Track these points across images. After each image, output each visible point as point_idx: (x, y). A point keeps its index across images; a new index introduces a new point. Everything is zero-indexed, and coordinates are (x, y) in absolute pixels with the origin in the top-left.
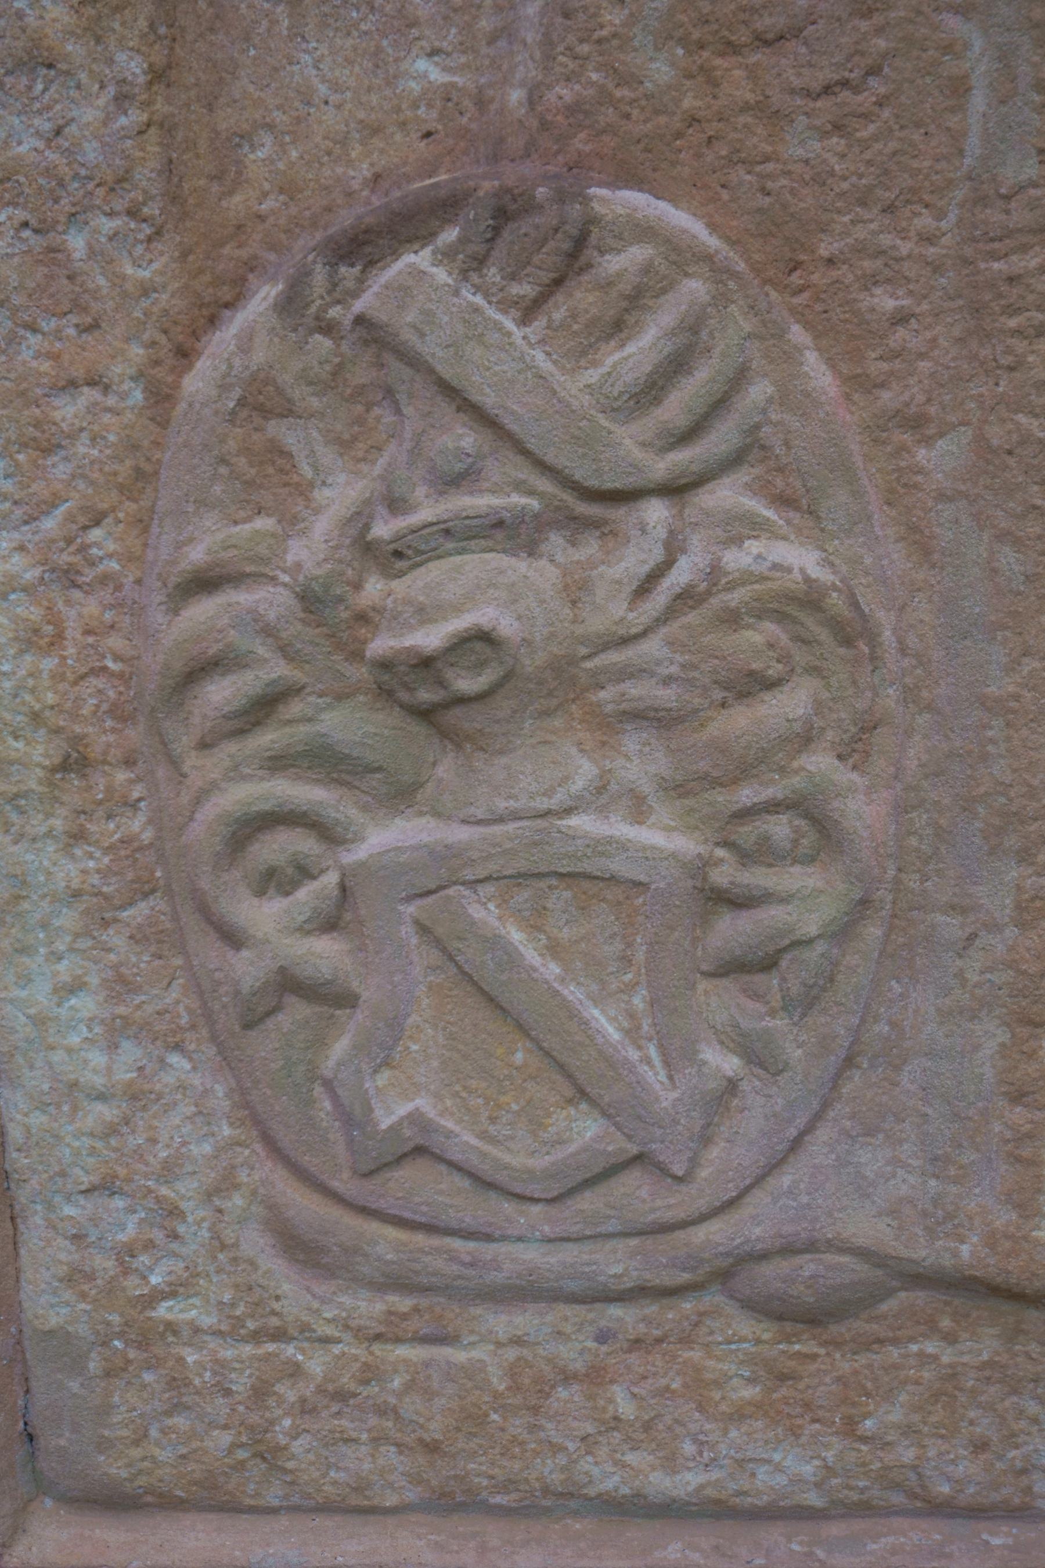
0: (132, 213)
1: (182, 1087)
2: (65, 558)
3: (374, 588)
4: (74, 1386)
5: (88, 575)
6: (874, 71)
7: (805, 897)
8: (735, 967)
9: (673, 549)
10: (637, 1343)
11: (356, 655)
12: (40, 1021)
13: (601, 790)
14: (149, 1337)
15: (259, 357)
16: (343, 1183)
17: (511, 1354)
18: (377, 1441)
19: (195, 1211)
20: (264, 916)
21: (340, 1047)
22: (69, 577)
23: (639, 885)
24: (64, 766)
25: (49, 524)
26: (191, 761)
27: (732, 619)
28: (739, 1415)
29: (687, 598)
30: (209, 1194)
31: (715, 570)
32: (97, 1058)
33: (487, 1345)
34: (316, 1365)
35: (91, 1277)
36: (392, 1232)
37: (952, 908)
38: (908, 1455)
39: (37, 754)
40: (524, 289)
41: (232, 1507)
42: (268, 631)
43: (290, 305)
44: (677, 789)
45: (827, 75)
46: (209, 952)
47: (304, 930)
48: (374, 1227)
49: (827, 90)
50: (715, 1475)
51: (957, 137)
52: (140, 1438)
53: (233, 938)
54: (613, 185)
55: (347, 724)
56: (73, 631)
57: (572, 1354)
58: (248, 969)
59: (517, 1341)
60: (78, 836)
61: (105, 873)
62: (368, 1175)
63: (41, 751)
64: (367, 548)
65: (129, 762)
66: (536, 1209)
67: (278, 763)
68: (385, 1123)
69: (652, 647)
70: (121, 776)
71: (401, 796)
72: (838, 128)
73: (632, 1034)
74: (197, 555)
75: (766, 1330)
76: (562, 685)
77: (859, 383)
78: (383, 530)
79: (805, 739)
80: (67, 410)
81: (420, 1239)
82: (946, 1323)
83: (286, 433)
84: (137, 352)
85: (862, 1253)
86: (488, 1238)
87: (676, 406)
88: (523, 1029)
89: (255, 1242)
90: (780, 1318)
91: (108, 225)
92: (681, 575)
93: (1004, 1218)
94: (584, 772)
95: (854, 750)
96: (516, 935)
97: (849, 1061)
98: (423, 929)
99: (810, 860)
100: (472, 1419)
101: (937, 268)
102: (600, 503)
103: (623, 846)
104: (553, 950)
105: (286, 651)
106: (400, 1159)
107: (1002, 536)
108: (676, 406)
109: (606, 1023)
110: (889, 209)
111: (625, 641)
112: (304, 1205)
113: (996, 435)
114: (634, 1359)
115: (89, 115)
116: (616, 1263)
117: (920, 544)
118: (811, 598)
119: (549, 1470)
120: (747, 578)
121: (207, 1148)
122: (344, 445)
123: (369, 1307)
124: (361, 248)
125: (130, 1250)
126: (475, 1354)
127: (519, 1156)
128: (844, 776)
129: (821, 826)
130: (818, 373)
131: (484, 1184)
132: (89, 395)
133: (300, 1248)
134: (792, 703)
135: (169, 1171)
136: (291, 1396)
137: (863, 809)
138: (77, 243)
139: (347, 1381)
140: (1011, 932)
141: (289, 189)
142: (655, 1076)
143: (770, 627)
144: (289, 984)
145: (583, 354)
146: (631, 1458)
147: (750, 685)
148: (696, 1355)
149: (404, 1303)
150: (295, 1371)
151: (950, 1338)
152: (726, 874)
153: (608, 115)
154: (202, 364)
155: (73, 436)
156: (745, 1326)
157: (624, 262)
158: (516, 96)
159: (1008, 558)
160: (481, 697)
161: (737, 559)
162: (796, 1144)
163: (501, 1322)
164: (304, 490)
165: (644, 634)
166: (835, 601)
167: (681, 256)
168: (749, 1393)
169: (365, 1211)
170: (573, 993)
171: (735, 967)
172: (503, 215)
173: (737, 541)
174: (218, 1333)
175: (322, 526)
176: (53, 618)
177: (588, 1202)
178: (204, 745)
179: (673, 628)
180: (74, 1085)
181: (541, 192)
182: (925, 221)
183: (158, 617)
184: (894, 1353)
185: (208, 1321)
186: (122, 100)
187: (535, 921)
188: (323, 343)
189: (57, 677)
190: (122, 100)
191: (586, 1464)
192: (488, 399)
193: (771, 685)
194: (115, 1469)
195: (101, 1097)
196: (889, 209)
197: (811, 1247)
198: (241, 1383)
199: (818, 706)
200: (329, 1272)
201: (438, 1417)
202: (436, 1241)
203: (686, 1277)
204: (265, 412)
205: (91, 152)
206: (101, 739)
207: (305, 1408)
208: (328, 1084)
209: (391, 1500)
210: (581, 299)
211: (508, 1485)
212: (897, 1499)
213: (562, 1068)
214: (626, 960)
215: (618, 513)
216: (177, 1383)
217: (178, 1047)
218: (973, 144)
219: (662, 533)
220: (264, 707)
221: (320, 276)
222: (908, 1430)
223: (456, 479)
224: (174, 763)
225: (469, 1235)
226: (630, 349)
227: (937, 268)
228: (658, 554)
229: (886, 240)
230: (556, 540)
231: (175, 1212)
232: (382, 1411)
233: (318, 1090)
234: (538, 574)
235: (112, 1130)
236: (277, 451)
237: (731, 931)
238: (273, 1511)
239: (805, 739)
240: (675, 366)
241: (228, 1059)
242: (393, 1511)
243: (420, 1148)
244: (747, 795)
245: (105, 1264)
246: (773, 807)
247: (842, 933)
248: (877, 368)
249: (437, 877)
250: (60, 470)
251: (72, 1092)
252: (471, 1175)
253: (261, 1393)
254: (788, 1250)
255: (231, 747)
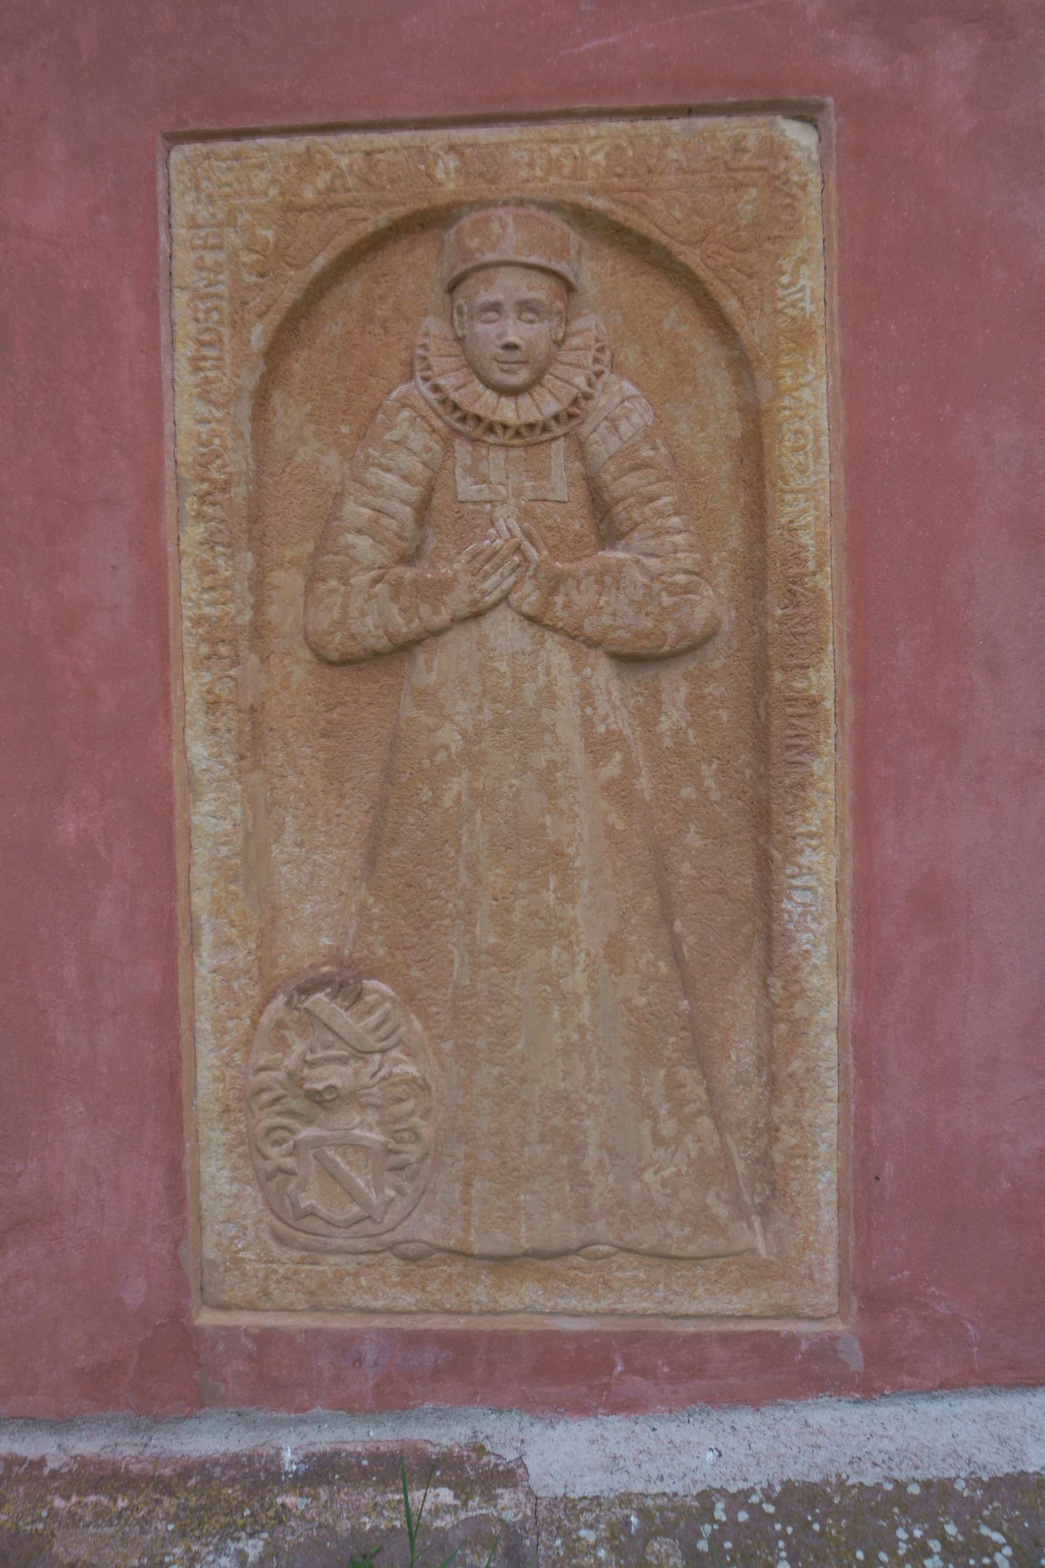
0: (250, 979)
1: (250, 1195)
2: (227, 1060)
3: (306, 1071)
4: (215, 1275)
5: (233, 1065)
6: (432, 957)
7: (412, 1152)
8: (393, 1169)
9: (381, 1066)
10: (368, 1266)
11: (301, 1087)
12: (213, 1177)
13: (361, 1123)
14: (237, 1262)
15: (280, 1015)
16: (291, 1221)
17: (334, 1268)
18: (297, 1291)
19: (251, 1228)
20: (274, 1152)
21: (292, 1186)
22: (228, 1065)
23: (370, 1148)
24: (224, 1111)
25: (224, 1051)
26: (256, 1113)
27: (394, 1085)
28: (395, 1285)
29: (383, 1079)
30: (255, 1224)
31: (390, 1073)
32: (227, 1187)
33: (328, 1265)
34: (281, 1270)
35: (222, 1245)
36: (303, 1235)
37: (449, 1155)
38: (439, 1297)
39: (217, 1108)
40: (346, 1004)
41: (256, 1309)
42: (279, 1082)
43: (289, 1003)
44: (380, 1124)
45: (420, 957)
46: (259, 1161)
47: (285, 1156)
48: (298, 1233)
49: (421, 961)
50: (388, 1301)
51: (452, 972)
52: (232, 1290)
53: (265, 1157)
54: (369, 979)
55: (297, 1104)
56: (228, 1077)
57: (351, 1268)
58: (269, 1166)
59: (336, 1265)
60: (226, 1129)
61: (233, 1139)
62: (298, 1219)
63: (218, 1107)
64: (305, 1062)
65: (241, 1111)
66: (342, 1230)
67: (279, 1114)
68: (303, 1206)
69: (375, 1090)
70: (238, 1115)
71: (310, 1121)
72: (423, 969)
73: (368, 1185)
74: (262, 1062)
75: (402, 1263)
76: (352, 1098)
77: (427, 1028)
78: (309, 1057)
79: (412, 1113)
80: (230, 1024)
81: (311, 1237)
82: (448, 1261)
83: (286, 1033)
84: (249, 1012)
85: (426, 1243)
86: (329, 1237)
87: (383, 1032)
88: (340, 1183)
89: (267, 1237)
90: (405, 1259)
91: (243, 981)
92: (383, 1072)
93: (461, 1234)
94: (357, 1119)
95: (425, 1116)
96: (339, 1159)
97: (423, 1193)
98: (315, 1156)
99: (414, 1142)
100: (323, 1285)
101: (447, 1001)
102: (362, 1054)
103: (367, 1138)
104: (348, 1163)
105: (283, 1087)
106: (306, 1216)
107: (461, 1066)
108: (383, 1032)
109: (361, 1183)
110: (435, 988)
111: (368, 1087)
112: (280, 1227)
113: (460, 1042)
114: (367, 1270)
115: (241, 956)
116: (362, 1244)
117: (442, 1066)
118: (414, 1080)
119: (343, 1300)
120: (398, 1075)
121: (255, 1211)
122: (300, 1036)
123: (296, 1255)
124: (307, 990)
125: (233, 1238)
126: (325, 1268)
127: (337, 1215)
128: (422, 1122)
129: (417, 1137)
130: (417, 1025)
131: (328, 1223)
132: (236, 1021)
133: (278, 1238)
134: (409, 1105)
135: (244, 1217)
136: (274, 1278)
137: (427, 1131)
138: (235, 985)
139: (289, 1274)
140: (463, 1162)
141: (289, 968)
142: (373, 1196)
143: (405, 1087)
144: (280, 1170)
145: (360, 1019)
146: (366, 1297)
147: (399, 1100)
148: (383, 1269)
149: (306, 1254)
150: (276, 1272)
151: (450, 1266)
152: (392, 1145)
153: (368, 962)
154: (265, 1015)
155: (232, 1030)
156: (396, 1261)
157: (370, 998)
158: (346, 952)
159: (462, 1071)
160: (333, 1100)
161: (396, 1070)
162: (409, 1214)
163: (332, 1259)
164: (289, 1046)
165: (373, 1086)
166: (420, 1081)
167: (384, 997)
168: (397, 1279)
169: (297, 1229)
170: (353, 1174)
171: (393, 1169)
172: (342, 985)
173: (396, 1065)
174: (255, 1261)
175: (294, 1056)
176: (224, 1076)
177: (355, 1228)
178: (261, 1109)
179: (381, 1085)
180: (221, 1194)
181: (351, 981)
182: (444, 991)
183: (251, 1077)
184: (435, 1269)
185: (253, 1258)
186: (250, 953)
187: (344, 1156)
188: (296, 1013)
189: (223, 1089)
190: (250, 953)
191: (353, 1298)
192: (337, 1029)
193: (404, 1100)
194: (225, 1298)
195: (228, 1197)
196: (435, 988)
197: (412, 1241)
198: (261, 1275)
199: (416, 1105)
200: (286, 1245)
201: (757, 1168)
202: (314, 1237)
203: (380, 1248)
204: (281, 1028)
205: (241, 965)
206: (233, 1105)
207: (278, 1282)
208: (289, 1196)
209: (300, 1308)
210: (360, 1006)
211: (331, 1304)
212: (437, 1309)
213: (349, 1193)
214: (366, 1166)
215: (368, 1056)
216: (244, 1274)
217: (249, 1185)
218: (455, 974)
219: (378, 1063)
220: (277, 1100)
221: (296, 997)
222: (439, 1290)
223: (327, 1047)
224: (253, 1113)
225: (324, 1236)
226: (372, 1018)
227: (447, 1001)
228: (377, 1068)
229: (434, 995)
230: (352, 1062)
231: (245, 1228)
232: (299, 1283)
233: (286, 1197)
234: (348, 1070)
235: (229, 1206)
236: (283, 1037)
237: (394, 1160)
238: (268, 1310)
239: (412, 1113)
240: (383, 1022)
241: (262, 1188)
242: (300, 1311)
243: (311, 1213)
244: (398, 1127)
245: (226, 1242)
246: (404, 1130)
247: (421, 1161)
248: (431, 1024)
249: (319, 1143)
250: (227, 1038)
251: (219, 1196)
252: (325, 1220)
253: (266, 1277)
254: (407, 1242)
255: (268, 1109)
